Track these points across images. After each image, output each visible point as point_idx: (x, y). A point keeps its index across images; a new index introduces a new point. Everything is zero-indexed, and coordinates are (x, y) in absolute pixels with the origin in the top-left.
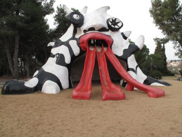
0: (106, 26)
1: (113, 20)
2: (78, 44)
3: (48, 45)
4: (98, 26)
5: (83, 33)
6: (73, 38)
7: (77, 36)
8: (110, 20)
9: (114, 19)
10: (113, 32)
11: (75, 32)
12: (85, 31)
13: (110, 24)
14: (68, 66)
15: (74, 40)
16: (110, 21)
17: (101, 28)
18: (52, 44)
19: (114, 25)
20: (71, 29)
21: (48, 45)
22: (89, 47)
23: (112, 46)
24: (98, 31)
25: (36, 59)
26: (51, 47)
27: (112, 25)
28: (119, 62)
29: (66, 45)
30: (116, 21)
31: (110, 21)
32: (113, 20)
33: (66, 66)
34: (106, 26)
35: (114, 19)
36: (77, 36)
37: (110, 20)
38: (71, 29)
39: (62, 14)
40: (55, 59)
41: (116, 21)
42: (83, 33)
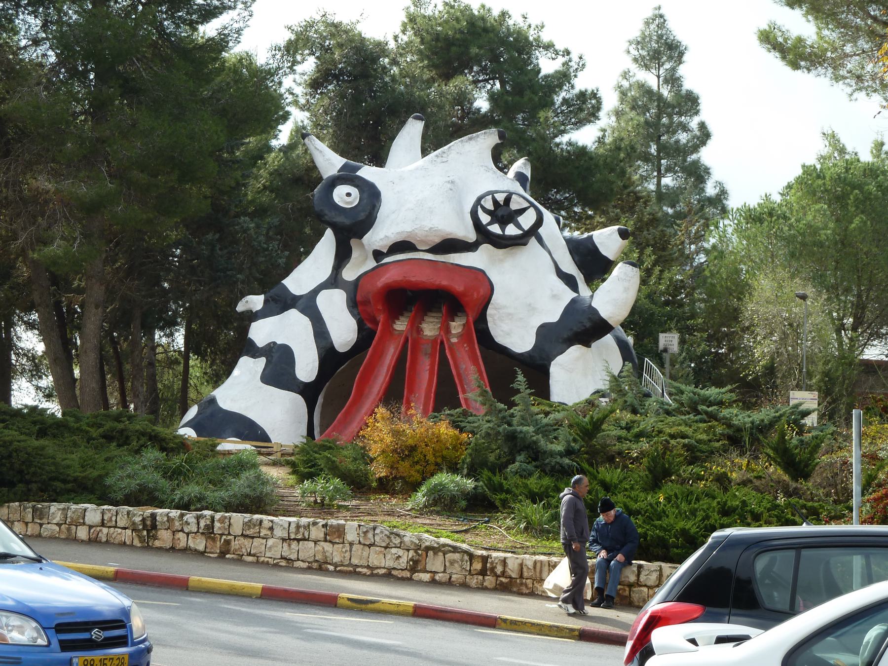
0: (471, 235)
1: (495, 202)
2: (354, 305)
3: (240, 307)
4: (426, 236)
5: (371, 264)
6: (334, 281)
7: (350, 274)
8: (482, 202)
9: (500, 198)
10: (501, 251)
11: (342, 256)
12: (378, 255)
13: (485, 218)
14: (309, 392)
15: (336, 287)
16: (483, 208)
17: (437, 240)
18: (256, 302)
19: (503, 223)
20: (326, 246)
21: (240, 307)
22: (77, 380)
23: (490, 311)
24: (429, 251)
25: (187, 359)
26: (252, 316)
27: (490, 224)
28: (474, 135)
29: (302, 311)
30: (514, 206)
31: (483, 208)
32: (495, 202)
33: (301, 393)
34: (471, 235)
35: (500, 198)
36: (350, 274)
37: (482, 202)
38: (326, 246)
39: (54, 79)
40: (260, 363)
41: (514, 206)
42: (371, 264)
